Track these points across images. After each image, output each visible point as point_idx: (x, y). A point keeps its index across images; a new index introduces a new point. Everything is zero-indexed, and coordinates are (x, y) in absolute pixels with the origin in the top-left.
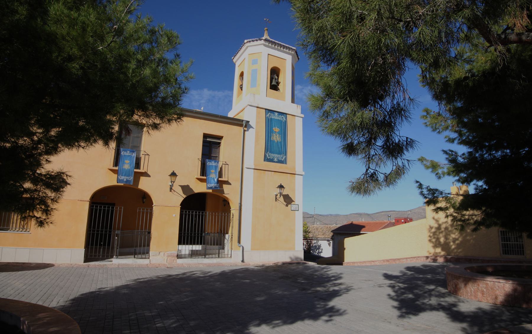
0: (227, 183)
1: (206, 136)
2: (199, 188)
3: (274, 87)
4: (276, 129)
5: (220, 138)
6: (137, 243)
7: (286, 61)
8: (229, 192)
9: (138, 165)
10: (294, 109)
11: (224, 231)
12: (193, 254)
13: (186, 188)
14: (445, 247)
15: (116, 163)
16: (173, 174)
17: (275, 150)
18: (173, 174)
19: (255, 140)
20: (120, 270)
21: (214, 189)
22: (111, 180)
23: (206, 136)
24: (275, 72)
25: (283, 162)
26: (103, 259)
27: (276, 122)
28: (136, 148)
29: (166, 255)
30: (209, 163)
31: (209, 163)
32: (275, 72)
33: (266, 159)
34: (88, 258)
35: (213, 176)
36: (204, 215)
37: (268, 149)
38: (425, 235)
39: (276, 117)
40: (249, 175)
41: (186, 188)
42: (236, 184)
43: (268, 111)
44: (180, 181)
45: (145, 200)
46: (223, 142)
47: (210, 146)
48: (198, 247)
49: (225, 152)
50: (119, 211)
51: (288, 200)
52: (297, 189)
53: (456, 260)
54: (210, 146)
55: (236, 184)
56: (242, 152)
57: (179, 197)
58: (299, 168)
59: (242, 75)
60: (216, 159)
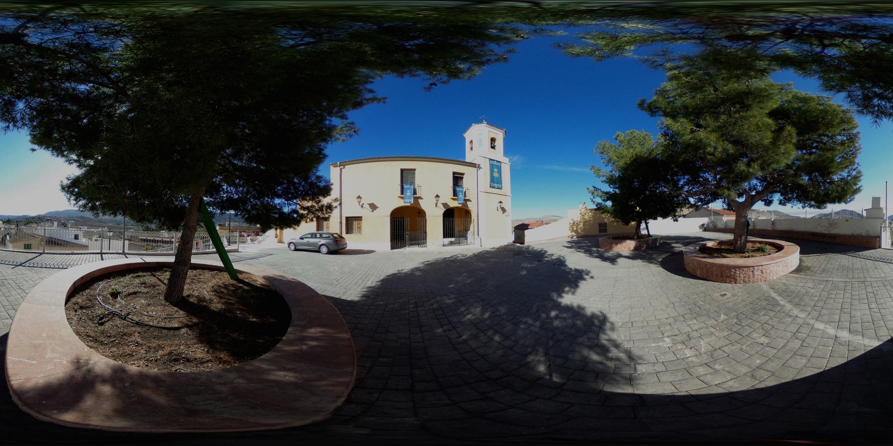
0: (469, 200)
1: (454, 173)
2: (453, 204)
3: (493, 147)
4: (495, 170)
5: (463, 174)
6: (419, 238)
7: (499, 135)
8: (471, 206)
9: (415, 193)
10: (506, 160)
11: (467, 230)
12: (451, 243)
13: (445, 205)
14: (576, 232)
15: (402, 193)
16: (437, 196)
17: (495, 182)
18: (437, 196)
19: (485, 174)
20: (411, 258)
21: (463, 204)
22: (401, 203)
23: (454, 173)
24: (493, 140)
25: (501, 188)
26: (401, 248)
27: (495, 166)
28: (413, 183)
29: (436, 246)
30: (458, 189)
31: (458, 189)
32: (493, 140)
33: (491, 187)
34: (392, 248)
35: (461, 196)
36: (456, 221)
37: (493, 180)
38: (568, 226)
39: (495, 163)
40: (482, 196)
41: (445, 205)
42: (474, 201)
43: (490, 160)
44: (442, 200)
45: (421, 213)
46: (465, 177)
47: (457, 179)
48: (453, 239)
49: (466, 183)
50: (408, 222)
51: (504, 210)
52: (507, 205)
53: (582, 237)
54: (457, 179)
55: (474, 201)
56: (476, 183)
57: (442, 210)
58: (509, 192)
59: (471, 142)
60: (461, 186)
